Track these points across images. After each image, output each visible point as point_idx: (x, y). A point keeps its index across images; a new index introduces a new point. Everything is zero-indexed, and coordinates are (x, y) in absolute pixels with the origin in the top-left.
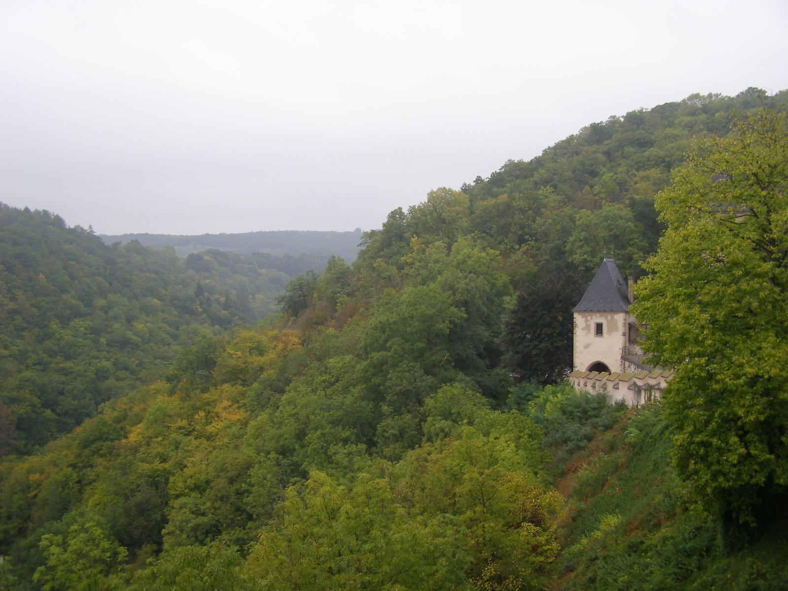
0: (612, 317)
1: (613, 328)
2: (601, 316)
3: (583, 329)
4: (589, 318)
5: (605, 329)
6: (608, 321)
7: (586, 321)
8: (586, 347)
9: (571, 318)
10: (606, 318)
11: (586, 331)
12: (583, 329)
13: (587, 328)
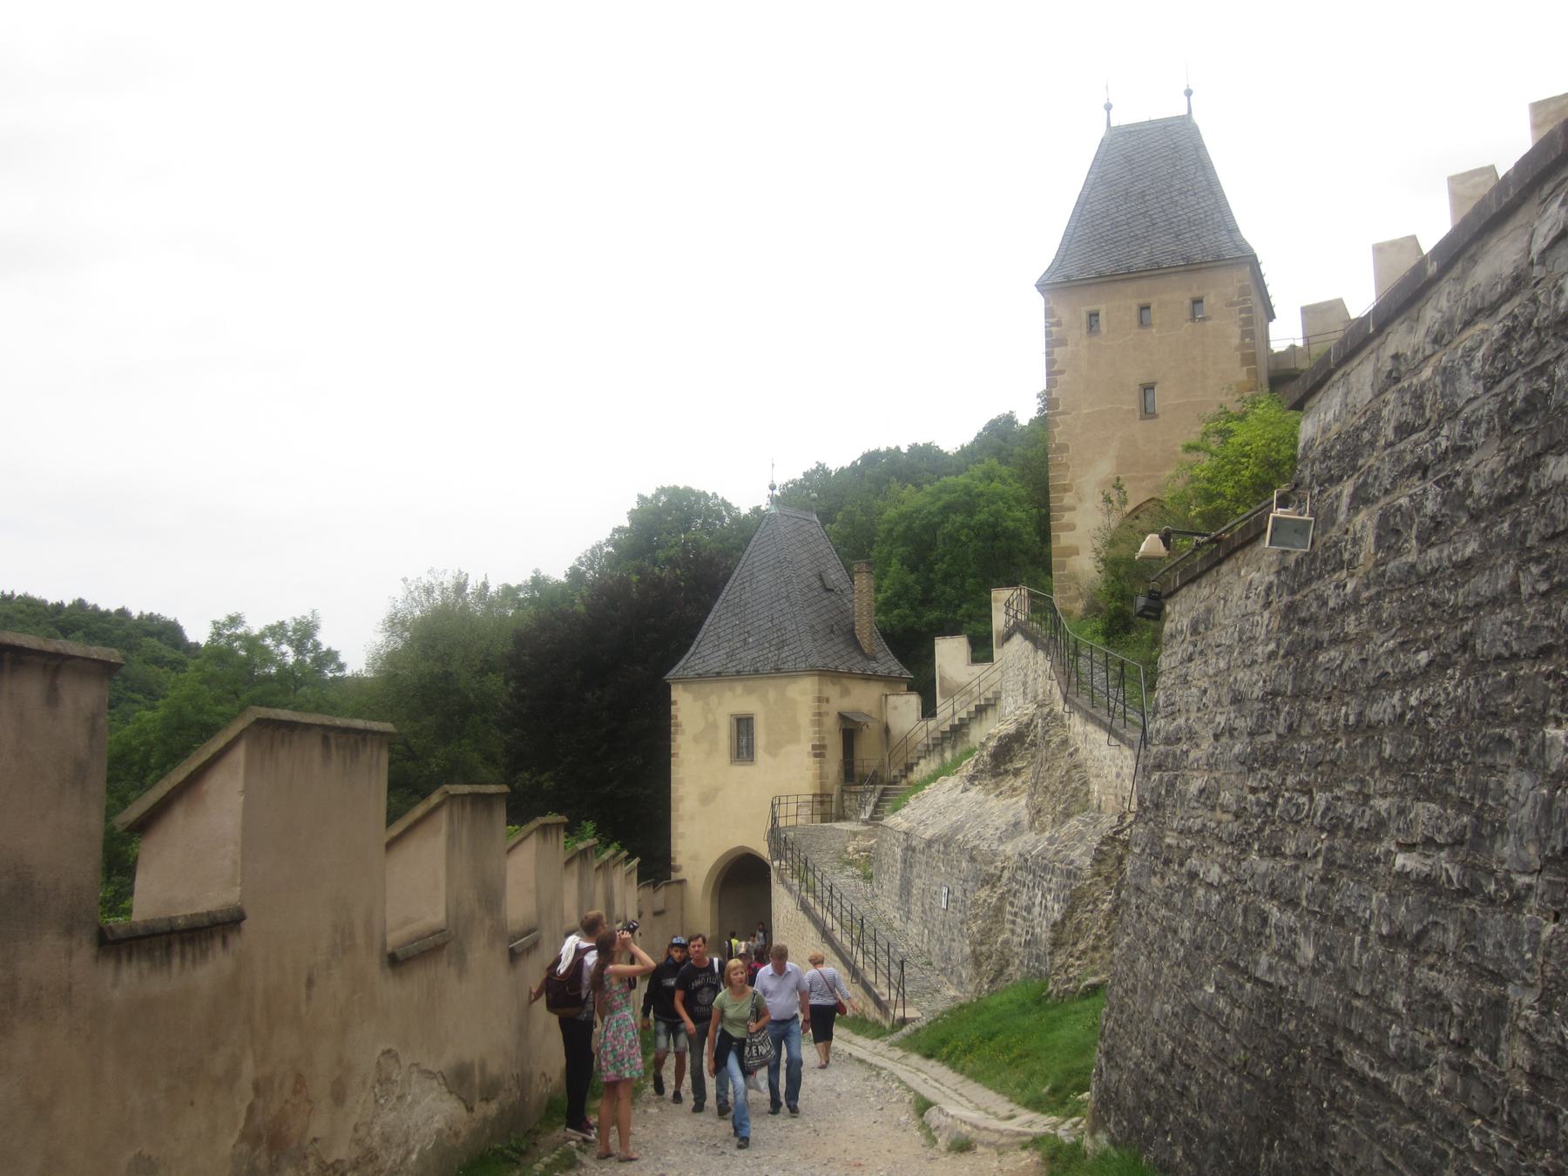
3: (697, 739)
9: (665, 702)
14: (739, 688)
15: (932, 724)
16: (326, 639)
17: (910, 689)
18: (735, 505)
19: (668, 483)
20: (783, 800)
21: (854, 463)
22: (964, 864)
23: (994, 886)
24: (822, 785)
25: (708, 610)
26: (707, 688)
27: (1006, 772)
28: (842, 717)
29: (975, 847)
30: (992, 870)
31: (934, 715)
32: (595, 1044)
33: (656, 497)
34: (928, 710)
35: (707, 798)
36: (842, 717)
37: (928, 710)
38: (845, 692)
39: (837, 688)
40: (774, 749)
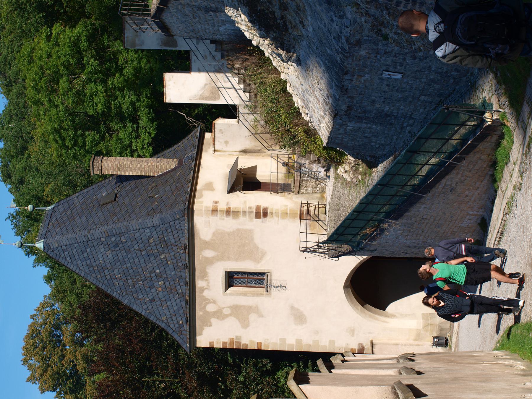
0: (207, 245)
1: (245, 243)
2: (205, 275)
3: (245, 324)
4: (210, 308)
6: (220, 258)
7: (219, 315)
8: (300, 318)
9: (209, 352)
10: (210, 261)
11: (252, 317)
12: (245, 324)
13: (240, 313)
14: (199, 283)
15: (241, 110)
16: (30, 324)
17: (210, 128)
18: (42, 300)
19: (19, 355)
20: (304, 245)
21: (10, 191)
22: (363, 52)
23: (382, 24)
24: (292, 215)
25: (129, 309)
26: (199, 313)
27: (283, 18)
28: (232, 189)
29: (348, 41)
30: (369, 26)
31: (234, 108)
32: (437, 15)
33: (30, 368)
34: (230, 112)
35: (300, 318)
36: (232, 189)
37: (230, 112)
38: (210, 187)
39: (206, 193)
40: (256, 253)
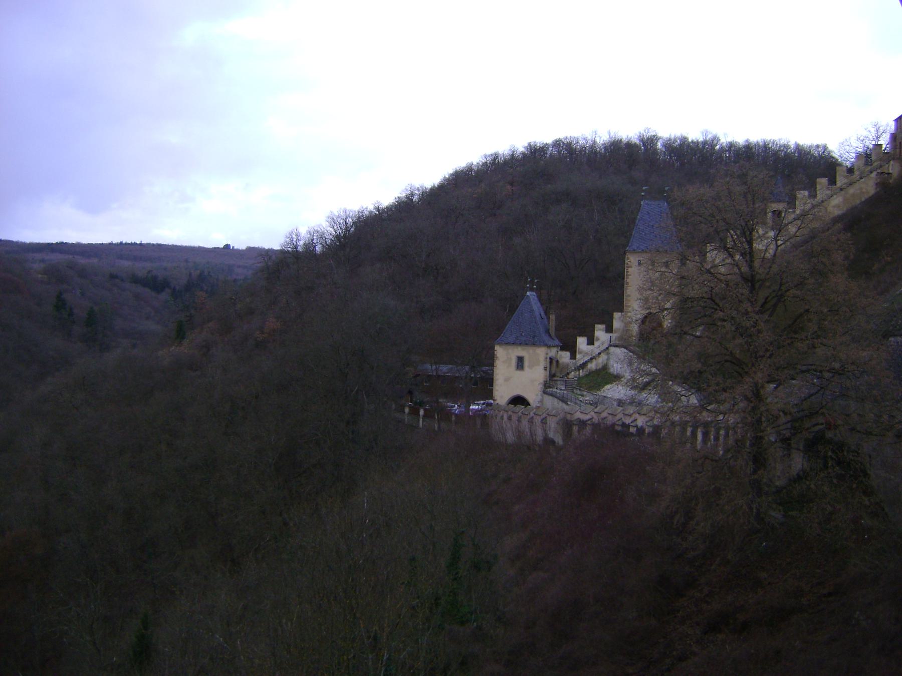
5: (526, 363)
40: (531, 367)
